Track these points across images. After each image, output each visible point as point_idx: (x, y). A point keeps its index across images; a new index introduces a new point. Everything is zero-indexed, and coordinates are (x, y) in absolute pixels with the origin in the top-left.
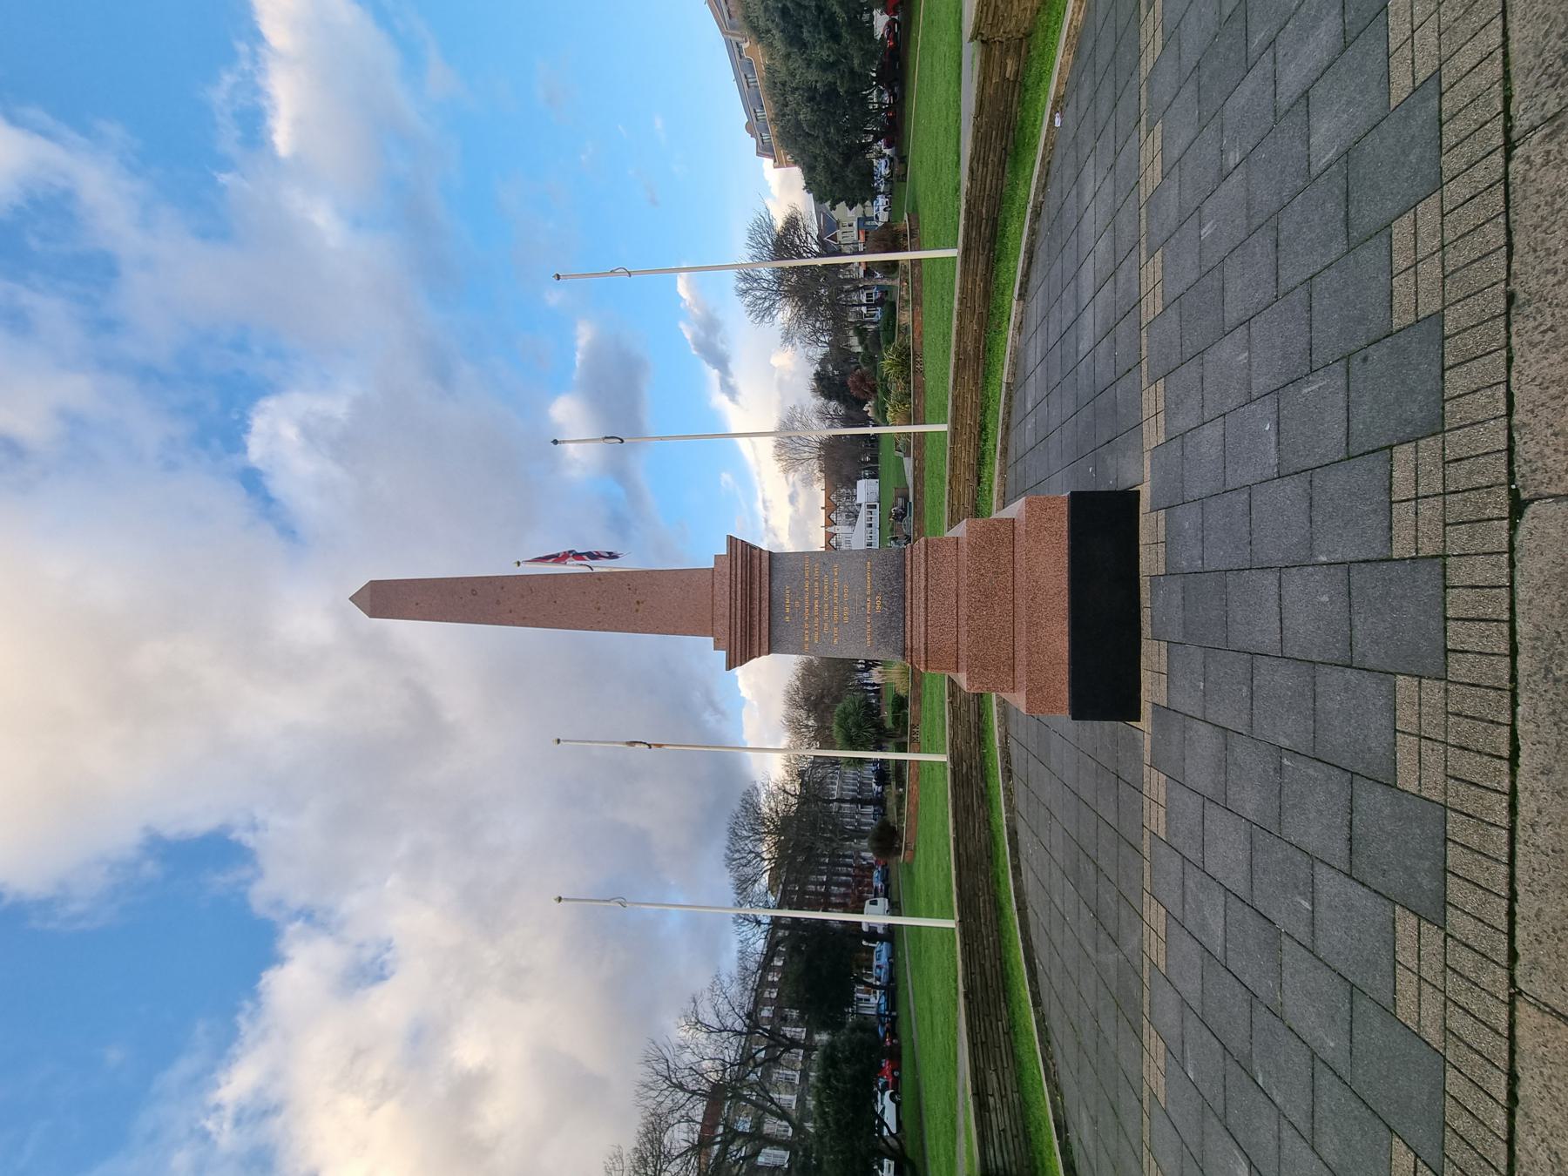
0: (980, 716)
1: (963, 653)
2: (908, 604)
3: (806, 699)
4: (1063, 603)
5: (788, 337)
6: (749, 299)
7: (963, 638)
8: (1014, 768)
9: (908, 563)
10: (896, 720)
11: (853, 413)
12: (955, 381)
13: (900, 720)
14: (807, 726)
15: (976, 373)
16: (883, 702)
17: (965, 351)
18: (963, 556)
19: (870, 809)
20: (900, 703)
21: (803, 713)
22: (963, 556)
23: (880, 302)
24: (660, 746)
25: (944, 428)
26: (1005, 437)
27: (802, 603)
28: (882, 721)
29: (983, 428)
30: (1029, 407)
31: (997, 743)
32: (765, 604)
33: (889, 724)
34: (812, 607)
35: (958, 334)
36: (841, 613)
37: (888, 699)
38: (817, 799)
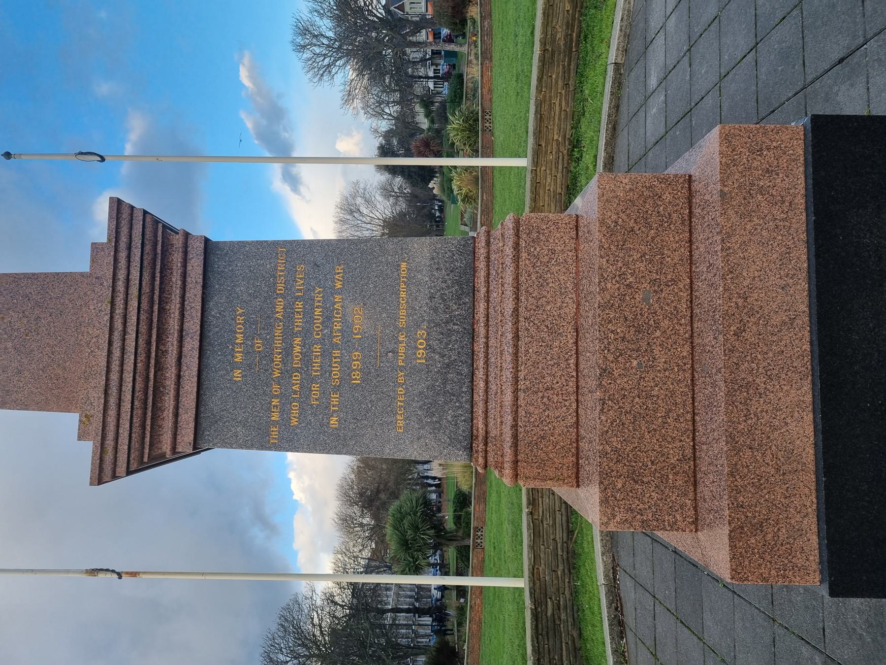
0: (570, 532)
1: (591, 447)
2: (479, 347)
3: (361, 495)
4: (799, 342)
5: (349, 97)
6: (307, 55)
7: (591, 417)
8: (629, 620)
9: (481, 265)
10: (457, 519)
11: (418, 191)
12: (540, 79)
13: (463, 520)
14: (361, 525)
15: (566, 71)
16: (444, 496)
17: (553, 40)
18: (591, 248)
19: (427, 620)
20: (463, 500)
21: (356, 509)
22: (591, 248)
23: (446, 77)
24: (134, 574)
25: (522, 162)
26: (611, 143)
27: (269, 343)
28: (441, 521)
29: (575, 144)
30: (653, 82)
31: (601, 580)
32: (192, 345)
33: (450, 525)
34: (288, 352)
35: (546, 14)
36: (346, 367)
37: (450, 494)
38: (367, 608)
